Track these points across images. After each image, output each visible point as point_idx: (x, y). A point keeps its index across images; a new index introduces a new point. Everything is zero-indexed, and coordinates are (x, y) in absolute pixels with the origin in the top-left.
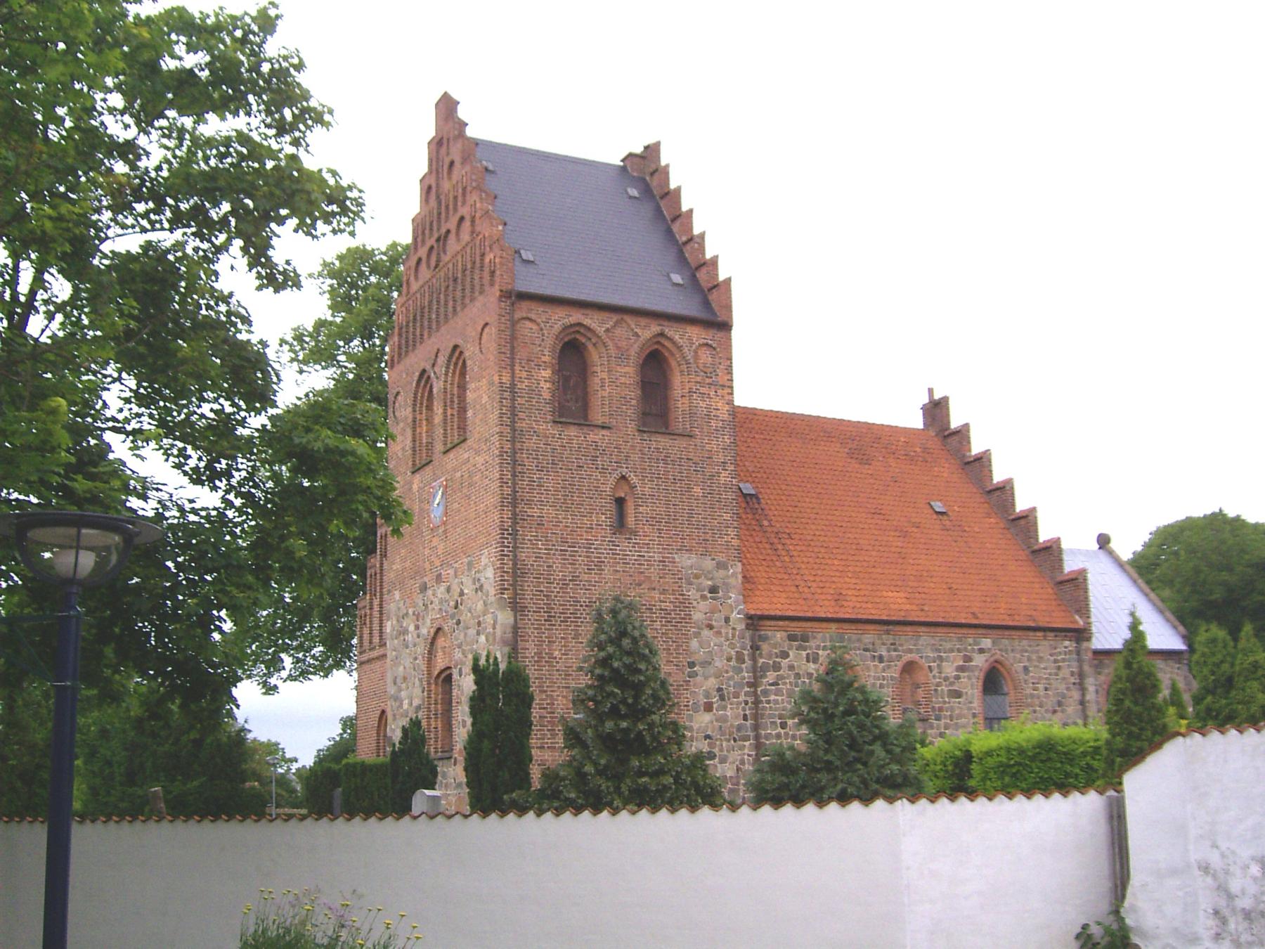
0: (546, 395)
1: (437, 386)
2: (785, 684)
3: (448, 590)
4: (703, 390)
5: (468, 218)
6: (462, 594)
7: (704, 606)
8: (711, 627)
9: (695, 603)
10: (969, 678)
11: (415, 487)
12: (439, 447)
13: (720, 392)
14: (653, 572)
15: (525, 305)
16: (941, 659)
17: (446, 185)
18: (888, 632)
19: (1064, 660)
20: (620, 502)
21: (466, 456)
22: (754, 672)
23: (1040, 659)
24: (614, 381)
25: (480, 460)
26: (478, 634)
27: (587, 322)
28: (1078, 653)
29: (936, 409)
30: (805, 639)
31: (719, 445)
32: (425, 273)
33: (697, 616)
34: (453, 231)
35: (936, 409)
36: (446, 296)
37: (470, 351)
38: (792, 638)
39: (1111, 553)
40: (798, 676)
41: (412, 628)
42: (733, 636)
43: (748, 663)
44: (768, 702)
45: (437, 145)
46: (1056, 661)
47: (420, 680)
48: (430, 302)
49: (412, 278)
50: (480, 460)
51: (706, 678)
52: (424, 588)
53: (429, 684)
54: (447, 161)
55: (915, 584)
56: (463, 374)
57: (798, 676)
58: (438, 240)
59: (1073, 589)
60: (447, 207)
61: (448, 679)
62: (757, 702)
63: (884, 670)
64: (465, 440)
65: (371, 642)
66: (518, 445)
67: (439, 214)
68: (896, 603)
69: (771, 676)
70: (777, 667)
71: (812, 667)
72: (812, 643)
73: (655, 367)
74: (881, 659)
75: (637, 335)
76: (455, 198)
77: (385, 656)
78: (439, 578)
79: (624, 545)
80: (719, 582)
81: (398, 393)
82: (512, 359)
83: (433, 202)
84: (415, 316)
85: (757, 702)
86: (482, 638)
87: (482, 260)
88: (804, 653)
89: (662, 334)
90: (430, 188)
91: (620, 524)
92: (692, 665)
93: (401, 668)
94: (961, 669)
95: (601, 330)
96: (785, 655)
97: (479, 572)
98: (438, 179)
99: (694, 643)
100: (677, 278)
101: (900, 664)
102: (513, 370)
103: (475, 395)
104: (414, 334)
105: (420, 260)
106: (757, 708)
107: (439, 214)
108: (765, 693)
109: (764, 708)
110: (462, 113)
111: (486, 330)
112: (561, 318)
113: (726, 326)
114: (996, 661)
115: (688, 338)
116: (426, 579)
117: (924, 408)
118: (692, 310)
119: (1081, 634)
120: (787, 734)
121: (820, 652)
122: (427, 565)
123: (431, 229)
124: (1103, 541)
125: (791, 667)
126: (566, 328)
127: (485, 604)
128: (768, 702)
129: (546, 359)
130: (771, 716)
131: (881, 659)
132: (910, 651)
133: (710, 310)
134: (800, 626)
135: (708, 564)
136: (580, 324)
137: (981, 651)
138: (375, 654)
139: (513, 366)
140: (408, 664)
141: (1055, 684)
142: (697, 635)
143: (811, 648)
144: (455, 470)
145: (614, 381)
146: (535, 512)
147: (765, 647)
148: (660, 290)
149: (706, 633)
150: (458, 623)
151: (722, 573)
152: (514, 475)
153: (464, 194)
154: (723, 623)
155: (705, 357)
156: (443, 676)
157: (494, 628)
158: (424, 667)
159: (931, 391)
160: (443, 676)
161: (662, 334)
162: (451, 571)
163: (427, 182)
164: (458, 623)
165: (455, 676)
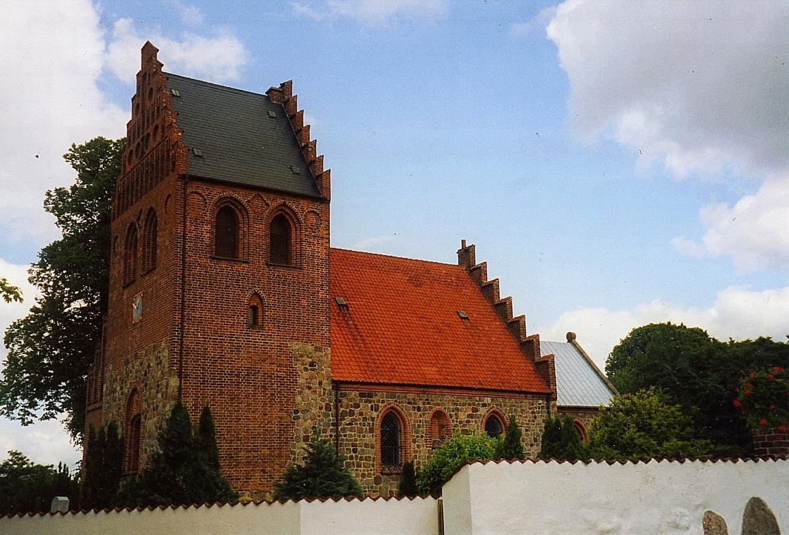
0: (207, 241)
1: (140, 233)
2: (357, 424)
3: (141, 364)
4: (311, 240)
5: (160, 126)
6: (149, 366)
7: (305, 374)
8: (310, 388)
9: (300, 373)
10: (476, 422)
11: (125, 297)
12: (139, 272)
13: (320, 241)
14: (274, 353)
15: (195, 184)
16: (458, 409)
17: (148, 104)
18: (424, 392)
19: (538, 412)
20: (255, 309)
21: (155, 278)
22: (337, 417)
23: (522, 411)
24: (256, 233)
25: (163, 281)
26: (157, 392)
27: (235, 195)
28: (548, 408)
29: (466, 253)
30: (370, 396)
31: (319, 272)
32: (135, 160)
33: (300, 381)
34: (152, 134)
35: (466, 253)
36: (147, 176)
37: (160, 211)
38: (362, 395)
39: (575, 345)
40: (365, 419)
41: (118, 388)
42: (324, 394)
43: (334, 411)
44: (345, 436)
45: (142, 77)
46: (533, 413)
47: (122, 423)
48: (137, 179)
49: (127, 164)
50: (163, 281)
51: (305, 420)
52: (127, 363)
53: (127, 425)
54: (148, 89)
55: (443, 362)
56: (156, 225)
57: (365, 419)
58: (142, 140)
59: (545, 369)
60: (148, 120)
61: (139, 422)
62: (337, 436)
63: (420, 416)
64: (154, 269)
65: (95, 398)
66: (187, 273)
67: (143, 123)
68: (431, 373)
69: (348, 419)
70: (352, 413)
71: (375, 414)
72: (375, 399)
73: (282, 227)
74: (419, 409)
75: (267, 204)
76: (153, 113)
77: (100, 408)
78: (136, 357)
79: (257, 337)
80: (316, 359)
81: (117, 237)
82: (185, 217)
83: (140, 115)
84: (128, 188)
85: (337, 436)
86: (160, 395)
87: (168, 154)
88: (370, 405)
89: (284, 204)
90: (138, 104)
91: (254, 324)
92: (296, 412)
93: (110, 415)
94: (470, 416)
95: (244, 202)
96: (357, 406)
97: (159, 352)
98: (143, 100)
99: (299, 398)
100: (297, 170)
101: (431, 413)
102: (185, 226)
103: (162, 240)
104: (127, 199)
105: (132, 151)
106: (337, 440)
107: (143, 123)
108: (344, 430)
109: (342, 440)
110: (160, 57)
111: (170, 199)
112: (217, 194)
113: (326, 201)
114: (494, 412)
115: (301, 208)
116: (129, 356)
117: (459, 252)
118: (307, 191)
119: (550, 396)
120: (356, 456)
121: (380, 404)
122: (129, 348)
123: (139, 132)
124: (571, 337)
125: (361, 414)
126: (220, 199)
127: (162, 373)
128: (345, 436)
129: (207, 218)
130: (346, 445)
131: (419, 409)
132: (438, 405)
133: (315, 186)
134: (367, 388)
135: (310, 348)
136: (232, 197)
137: (484, 405)
138: (97, 405)
139: (185, 222)
140: (114, 412)
141: (533, 427)
142: (300, 393)
143: (374, 401)
144: (148, 288)
145: (256, 233)
146: (197, 315)
147: (345, 401)
148: (282, 176)
149: (307, 391)
150: (146, 385)
151: (318, 354)
152: (183, 291)
153: (158, 112)
154: (318, 385)
155: (312, 219)
156: (136, 419)
157: (167, 389)
158: (124, 414)
159: (463, 242)
160: (136, 419)
161: (284, 204)
162: (144, 352)
163: (136, 101)
164: (146, 385)
165: (143, 420)
